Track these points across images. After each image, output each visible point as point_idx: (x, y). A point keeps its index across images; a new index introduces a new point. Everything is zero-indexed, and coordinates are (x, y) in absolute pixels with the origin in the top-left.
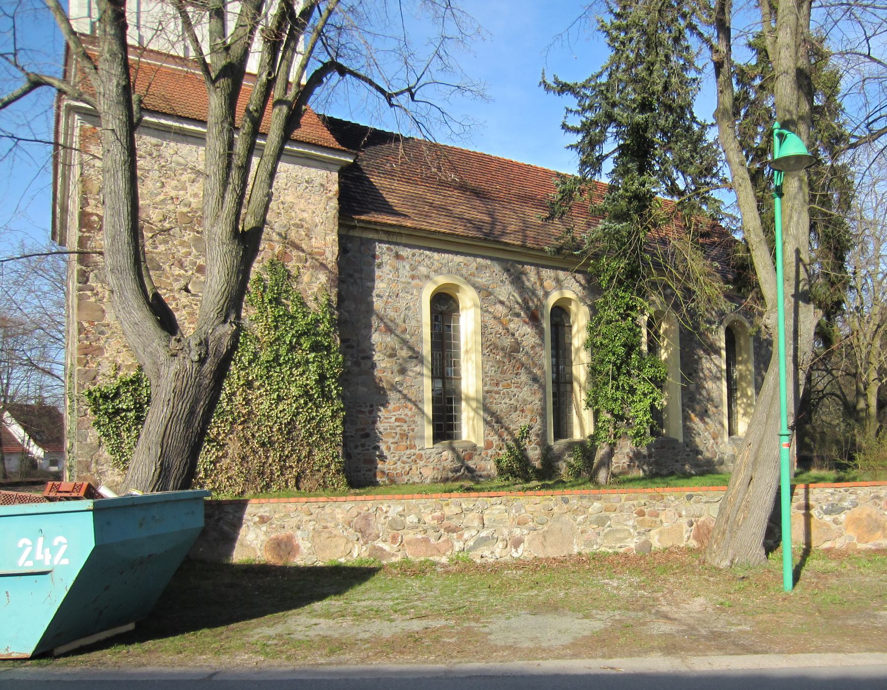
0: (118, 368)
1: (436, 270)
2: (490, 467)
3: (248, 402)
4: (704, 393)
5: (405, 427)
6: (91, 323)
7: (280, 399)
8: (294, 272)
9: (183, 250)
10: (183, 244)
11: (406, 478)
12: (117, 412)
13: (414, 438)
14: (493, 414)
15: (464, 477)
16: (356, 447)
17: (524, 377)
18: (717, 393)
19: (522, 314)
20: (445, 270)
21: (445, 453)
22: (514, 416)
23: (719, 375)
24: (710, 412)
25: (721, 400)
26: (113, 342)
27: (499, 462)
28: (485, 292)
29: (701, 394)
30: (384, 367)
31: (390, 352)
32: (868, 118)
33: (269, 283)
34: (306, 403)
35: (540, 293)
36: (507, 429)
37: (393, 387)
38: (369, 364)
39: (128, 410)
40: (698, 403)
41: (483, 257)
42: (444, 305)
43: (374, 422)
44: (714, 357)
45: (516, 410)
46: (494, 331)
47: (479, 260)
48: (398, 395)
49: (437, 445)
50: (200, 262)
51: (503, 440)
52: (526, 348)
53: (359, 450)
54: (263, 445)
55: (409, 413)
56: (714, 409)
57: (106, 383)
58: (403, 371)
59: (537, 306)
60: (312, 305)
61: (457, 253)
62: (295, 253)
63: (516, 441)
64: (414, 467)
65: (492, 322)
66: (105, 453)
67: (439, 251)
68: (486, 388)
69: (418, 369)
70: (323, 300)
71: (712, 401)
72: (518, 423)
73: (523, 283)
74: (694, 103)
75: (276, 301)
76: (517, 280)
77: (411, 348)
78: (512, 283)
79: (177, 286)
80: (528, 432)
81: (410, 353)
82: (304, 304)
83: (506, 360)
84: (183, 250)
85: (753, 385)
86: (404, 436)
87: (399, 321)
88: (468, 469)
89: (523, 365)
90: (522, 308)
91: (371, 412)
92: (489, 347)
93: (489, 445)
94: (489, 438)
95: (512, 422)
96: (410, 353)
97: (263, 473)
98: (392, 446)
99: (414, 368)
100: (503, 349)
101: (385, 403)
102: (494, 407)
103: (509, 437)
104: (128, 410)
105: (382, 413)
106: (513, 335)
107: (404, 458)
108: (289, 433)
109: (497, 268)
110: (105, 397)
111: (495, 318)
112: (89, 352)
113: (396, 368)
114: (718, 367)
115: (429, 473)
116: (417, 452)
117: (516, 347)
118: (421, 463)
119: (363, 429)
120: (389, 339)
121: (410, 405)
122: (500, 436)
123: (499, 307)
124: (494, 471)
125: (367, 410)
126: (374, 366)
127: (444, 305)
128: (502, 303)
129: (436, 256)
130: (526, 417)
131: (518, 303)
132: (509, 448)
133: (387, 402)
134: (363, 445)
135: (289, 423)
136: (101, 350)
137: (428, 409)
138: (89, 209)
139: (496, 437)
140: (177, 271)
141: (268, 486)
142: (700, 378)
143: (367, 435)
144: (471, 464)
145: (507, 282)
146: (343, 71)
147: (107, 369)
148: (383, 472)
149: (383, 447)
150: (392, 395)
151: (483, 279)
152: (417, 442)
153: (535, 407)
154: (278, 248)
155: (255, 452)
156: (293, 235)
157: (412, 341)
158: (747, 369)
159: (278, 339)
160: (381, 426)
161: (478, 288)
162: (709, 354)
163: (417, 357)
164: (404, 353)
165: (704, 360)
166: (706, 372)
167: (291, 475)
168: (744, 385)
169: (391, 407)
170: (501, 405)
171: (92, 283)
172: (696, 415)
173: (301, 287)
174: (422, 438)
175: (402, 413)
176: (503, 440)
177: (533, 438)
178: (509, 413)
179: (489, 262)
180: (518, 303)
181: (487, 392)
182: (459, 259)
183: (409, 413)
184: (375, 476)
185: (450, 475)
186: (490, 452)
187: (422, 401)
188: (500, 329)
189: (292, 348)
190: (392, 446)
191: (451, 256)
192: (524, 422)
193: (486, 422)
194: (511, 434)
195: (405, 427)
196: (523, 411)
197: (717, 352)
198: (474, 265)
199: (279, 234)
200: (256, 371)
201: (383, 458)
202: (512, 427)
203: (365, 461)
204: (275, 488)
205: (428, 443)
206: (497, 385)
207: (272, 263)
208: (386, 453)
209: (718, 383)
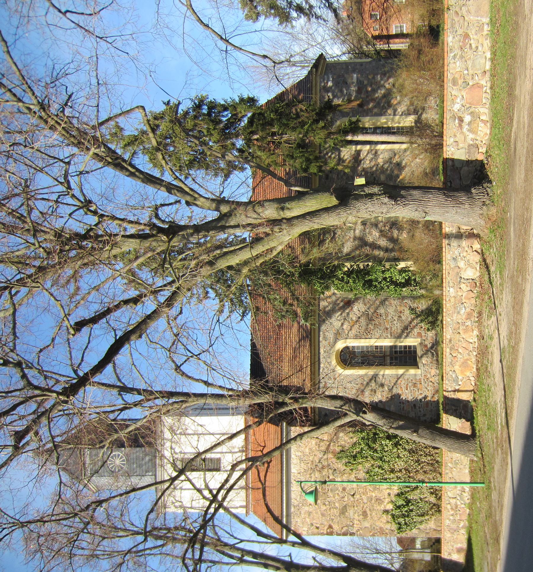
0: (388, 522)
1: (329, 363)
2: (431, 334)
3: (400, 471)
4: (386, 166)
5: (410, 384)
6: (370, 532)
7: (398, 457)
8: (340, 448)
9: (337, 497)
10: (334, 497)
11: (436, 384)
12: (406, 524)
13: (416, 379)
14: (403, 332)
15: (435, 349)
16: (420, 411)
17: (382, 311)
18: (386, 153)
19: (347, 311)
20: (329, 360)
21: (424, 362)
22: (404, 318)
23: (373, 152)
24: (399, 160)
25: (390, 150)
26: (377, 524)
27: (428, 330)
28: (338, 335)
29: (387, 170)
30: (381, 396)
31: (373, 393)
32: (5, 397)
33: (347, 460)
34: (400, 445)
35: (334, 298)
36: (411, 323)
37: (390, 390)
38: (380, 404)
39: (405, 520)
40: (393, 172)
41: (319, 337)
42: (348, 358)
43: (408, 401)
44: (362, 156)
45: (400, 317)
46: (358, 330)
47: (321, 339)
48: (394, 388)
49: (420, 365)
50: (341, 490)
51: (417, 325)
52: (366, 308)
53: (421, 409)
54: (419, 464)
55: (403, 382)
56: (397, 157)
57: (395, 527)
58: (382, 385)
59: (342, 301)
60: (355, 440)
61: (319, 353)
62: (331, 448)
63: (417, 317)
64: (431, 380)
65: (354, 332)
66: (422, 527)
67: (319, 364)
68: (389, 336)
69: (381, 377)
70: (351, 435)
71: (391, 158)
72: (407, 315)
73: (330, 310)
74: (211, 98)
75: (355, 457)
76: (329, 314)
77: (371, 380)
78: (331, 318)
79: (352, 499)
80: (412, 310)
81: (373, 381)
82: (355, 444)
83: (373, 322)
84: (337, 497)
85: (379, 118)
86: (415, 385)
87: (357, 387)
88: (432, 348)
89: (375, 311)
90: (344, 311)
91: (403, 403)
92: (366, 334)
93: (419, 335)
94: (416, 334)
95: (407, 320)
96: (373, 381)
97: (432, 464)
98: (420, 392)
99: (380, 379)
100: (368, 325)
101: (399, 395)
102: (399, 331)
103: (415, 321)
104: (405, 520)
105: (403, 397)
106: (359, 318)
107: (426, 385)
108: (414, 452)
109: (323, 328)
110: (399, 528)
111: (351, 330)
112: (382, 532)
113: (381, 389)
114: (368, 153)
115: (434, 371)
116: (423, 378)
117: (366, 314)
118: (429, 376)
119: (412, 408)
120: (367, 393)
121: (399, 382)
122: (414, 327)
123: (345, 327)
124: (434, 332)
125: (402, 405)
126: (380, 401)
127: (348, 358)
128: (342, 324)
129: (322, 365)
130: (404, 310)
131: (341, 314)
132: (422, 321)
133: (398, 394)
134: (419, 408)
135: (409, 452)
136: (381, 528)
137: (401, 371)
138: (325, 532)
139: (415, 330)
140: (346, 499)
141: (437, 462)
142: (377, 170)
143: (415, 405)
144: (429, 346)
145: (331, 321)
146: (274, 62)
147: (388, 526)
148: (433, 397)
149: (420, 397)
150: (395, 391)
151: (331, 336)
152: (418, 378)
153: (398, 303)
154: (330, 456)
155: (422, 468)
156: (323, 448)
157: (367, 380)
158: (369, 122)
159: (372, 457)
160: (410, 398)
161: (336, 341)
162: (361, 161)
163: (374, 377)
164: (373, 384)
165: (365, 166)
166: (373, 164)
167: (433, 451)
168: (379, 123)
169: (400, 392)
170: (397, 327)
171: (354, 531)
172: (401, 174)
173: (347, 445)
174: (415, 375)
175: (404, 386)
176: (417, 325)
177: (416, 305)
178: (402, 321)
179: (321, 333)
180: (341, 314)
181: (391, 335)
182: (322, 351)
183: (403, 382)
184: (434, 401)
185: (435, 358)
186: (423, 334)
187: (397, 375)
188: (356, 326)
189: (376, 451)
190: (420, 392)
191: (321, 357)
192: (407, 312)
193: (407, 337)
194: (413, 320)
195: (410, 384)
196: (401, 312)
197: (358, 153)
198: (324, 342)
199: (324, 455)
200: (386, 466)
201: (425, 397)
202: (410, 319)
203: (427, 406)
204: (438, 459)
205: (419, 372)
206: (387, 329)
207: (338, 458)
208: (423, 396)
209: (379, 153)
